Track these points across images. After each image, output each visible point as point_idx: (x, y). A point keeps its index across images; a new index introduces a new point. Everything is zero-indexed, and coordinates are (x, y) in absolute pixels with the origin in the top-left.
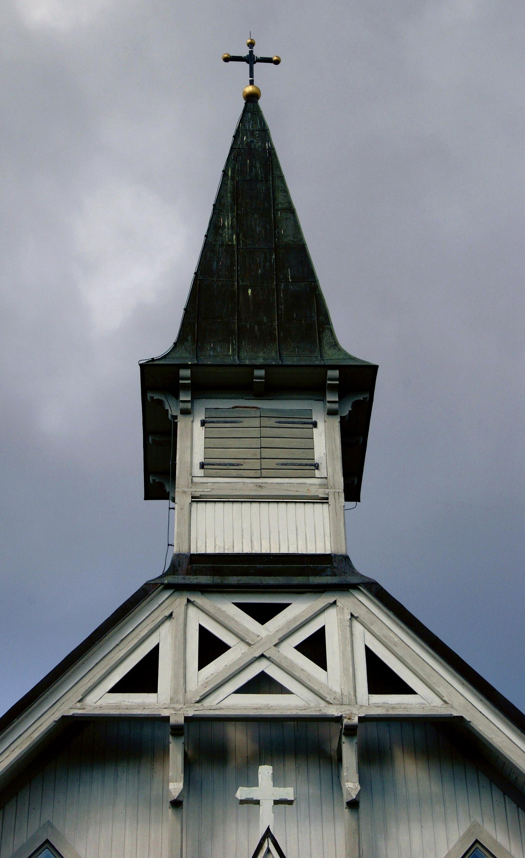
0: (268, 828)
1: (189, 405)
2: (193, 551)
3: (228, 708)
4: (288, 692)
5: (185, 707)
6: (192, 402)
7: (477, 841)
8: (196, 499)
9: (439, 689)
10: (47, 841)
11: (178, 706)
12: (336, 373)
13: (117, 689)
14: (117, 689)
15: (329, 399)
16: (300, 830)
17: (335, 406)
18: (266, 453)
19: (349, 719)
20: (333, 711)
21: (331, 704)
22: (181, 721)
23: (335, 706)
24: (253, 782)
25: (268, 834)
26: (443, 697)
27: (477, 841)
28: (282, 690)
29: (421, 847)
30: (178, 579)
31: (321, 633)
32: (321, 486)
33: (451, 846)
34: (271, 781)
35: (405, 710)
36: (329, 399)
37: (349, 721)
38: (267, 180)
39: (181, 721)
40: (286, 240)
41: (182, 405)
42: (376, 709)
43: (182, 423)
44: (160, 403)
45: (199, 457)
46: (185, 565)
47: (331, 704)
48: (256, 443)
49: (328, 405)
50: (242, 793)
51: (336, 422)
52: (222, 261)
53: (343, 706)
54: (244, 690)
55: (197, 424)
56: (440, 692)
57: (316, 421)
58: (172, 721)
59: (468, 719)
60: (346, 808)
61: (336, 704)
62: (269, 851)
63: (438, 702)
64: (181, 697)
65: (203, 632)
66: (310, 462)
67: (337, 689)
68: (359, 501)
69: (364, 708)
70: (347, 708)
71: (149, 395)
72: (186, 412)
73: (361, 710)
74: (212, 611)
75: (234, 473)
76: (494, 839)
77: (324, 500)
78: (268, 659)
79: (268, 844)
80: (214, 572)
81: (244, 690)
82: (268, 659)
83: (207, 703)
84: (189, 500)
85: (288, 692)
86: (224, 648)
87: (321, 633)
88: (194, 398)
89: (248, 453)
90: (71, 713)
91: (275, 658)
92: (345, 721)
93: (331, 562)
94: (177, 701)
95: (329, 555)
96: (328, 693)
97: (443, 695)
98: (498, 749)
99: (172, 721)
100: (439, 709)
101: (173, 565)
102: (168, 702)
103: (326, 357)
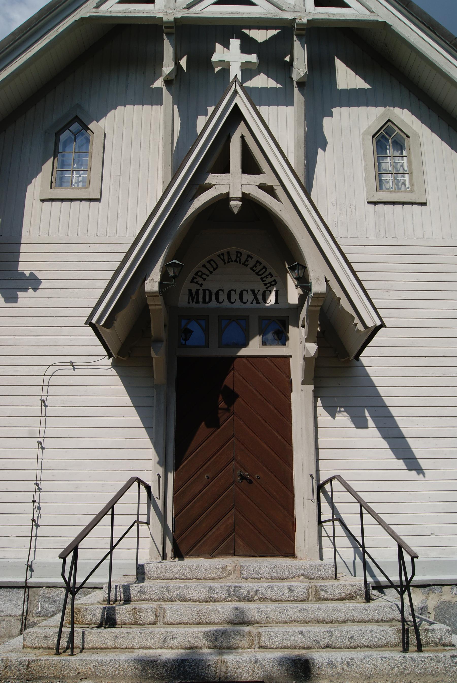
0: (236, 76)
3: (208, 13)
5: (175, 11)
7: (389, 120)
10: (77, 117)
19: (300, 20)
21: (287, 11)
23: (290, 13)
26: (372, 8)
27: (389, 120)
29: (349, 124)
34: (240, 168)
35: (343, 16)
37: (300, 21)
42: (320, 15)
47: (287, 11)
52: (239, 599)
53: (295, 13)
56: (370, 5)
59: (390, 24)
60: (296, 87)
61: (290, 12)
62: (236, 92)
64: (172, 5)
68: (228, 193)
69: (311, 14)
70: (299, 14)
73: (309, 16)
76: (401, 119)
83: (192, 10)
94: (169, 7)
96: (284, 4)
97: (372, 7)
98: (413, 44)
100: (368, 16)
102: (163, 8)
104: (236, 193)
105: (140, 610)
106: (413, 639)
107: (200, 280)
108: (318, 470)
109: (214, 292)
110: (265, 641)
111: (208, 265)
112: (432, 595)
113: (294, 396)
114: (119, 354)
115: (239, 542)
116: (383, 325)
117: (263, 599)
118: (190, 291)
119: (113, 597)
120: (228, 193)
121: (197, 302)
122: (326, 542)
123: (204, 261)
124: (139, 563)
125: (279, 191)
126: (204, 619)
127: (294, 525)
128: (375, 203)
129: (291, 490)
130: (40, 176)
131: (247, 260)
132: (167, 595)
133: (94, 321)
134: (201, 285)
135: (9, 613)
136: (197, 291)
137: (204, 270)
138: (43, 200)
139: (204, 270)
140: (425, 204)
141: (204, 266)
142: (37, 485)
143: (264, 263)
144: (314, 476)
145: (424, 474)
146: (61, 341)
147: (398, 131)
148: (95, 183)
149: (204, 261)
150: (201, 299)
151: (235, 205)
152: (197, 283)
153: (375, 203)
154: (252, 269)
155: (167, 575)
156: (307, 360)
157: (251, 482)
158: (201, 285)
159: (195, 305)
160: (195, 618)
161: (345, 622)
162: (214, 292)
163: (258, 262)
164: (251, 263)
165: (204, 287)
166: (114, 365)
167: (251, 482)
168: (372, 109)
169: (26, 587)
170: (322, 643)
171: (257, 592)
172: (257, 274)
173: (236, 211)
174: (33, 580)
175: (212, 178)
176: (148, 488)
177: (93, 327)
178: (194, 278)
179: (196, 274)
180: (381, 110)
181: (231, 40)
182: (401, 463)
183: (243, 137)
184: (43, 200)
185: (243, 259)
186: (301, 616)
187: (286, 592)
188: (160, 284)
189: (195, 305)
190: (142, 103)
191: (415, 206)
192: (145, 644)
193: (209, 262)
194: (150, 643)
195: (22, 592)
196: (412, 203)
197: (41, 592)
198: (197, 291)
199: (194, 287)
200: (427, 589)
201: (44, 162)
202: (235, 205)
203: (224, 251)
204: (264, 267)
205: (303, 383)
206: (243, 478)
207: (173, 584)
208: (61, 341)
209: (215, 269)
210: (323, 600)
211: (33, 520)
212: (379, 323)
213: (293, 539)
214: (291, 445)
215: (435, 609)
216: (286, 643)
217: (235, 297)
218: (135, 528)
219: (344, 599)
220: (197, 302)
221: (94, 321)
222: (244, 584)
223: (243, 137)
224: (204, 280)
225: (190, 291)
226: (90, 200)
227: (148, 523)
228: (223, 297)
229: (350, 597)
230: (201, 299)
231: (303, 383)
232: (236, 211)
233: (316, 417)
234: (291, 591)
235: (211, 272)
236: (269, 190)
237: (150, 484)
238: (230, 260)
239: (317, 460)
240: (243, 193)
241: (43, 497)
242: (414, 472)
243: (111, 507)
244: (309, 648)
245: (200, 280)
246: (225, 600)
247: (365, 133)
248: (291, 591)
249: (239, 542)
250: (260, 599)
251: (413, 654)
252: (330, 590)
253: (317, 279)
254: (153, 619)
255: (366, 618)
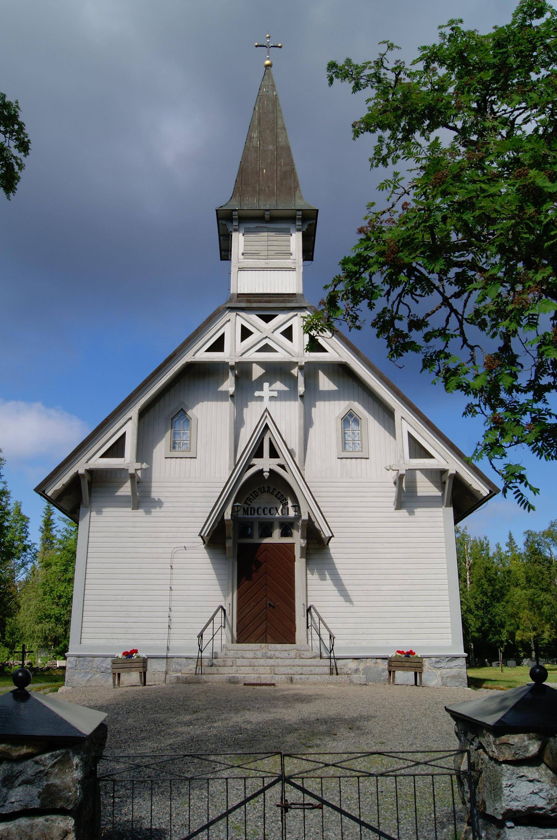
1: (237, 227)
2: (239, 292)
3: (252, 358)
4: (275, 351)
6: (239, 225)
8: (241, 269)
9: (337, 351)
11: (233, 358)
12: (300, 213)
13: (208, 350)
14: (208, 350)
15: (297, 224)
16: (229, 618)
17: (300, 227)
18: (270, 248)
20: (295, 360)
22: (234, 364)
24: (261, 389)
25: (266, 410)
28: (275, 351)
30: (232, 305)
31: (290, 328)
32: (293, 263)
33: (341, 411)
36: (297, 224)
38: (274, 112)
39: (234, 364)
40: (281, 144)
41: (234, 227)
43: (234, 235)
44: (225, 225)
45: (241, 250)
46: (235, 298)
48: (266, 243)
49: (297, 227)
50: (257, 394)
51: (300, 234)
54: (260, 350)
55: (241, 234)
57: (327, 66)
58: (230, 364)
62: (266, 416)
63: (337, 356)
64: (233, 354)
65: (243, 327)
66: (289, 252)
67: (297, 350)
68: (263, 469)
71: (220, 222)
72: (236, 230)
74: (246, 318)
75: (256, 257)
77: (294, 270)
78: (269, 338)
79: (266, 414)
80: (249, 301)
81: (260, 350)
82: (269, 338)
83: (244, 356)
84: (237, 269)
85: (275, 351)
86: (251, 333)
87: (290, 328)
88: (239, 223)
89: (262, 248)
90: (190, 361)
91: (271, 338)
92: (299, 364)
93: (296, 297)
95: (295, 294)
99: (230, 364)
101: (230, 299)
103: (297, 204)
104: (266, 469)
105: (226, 661)
106: (334, 671)
107: (249, 503)
108: (307, 601)
109: (256, 509)
110: (276, 672)
111: (253, 494)
112: (362, 663)
113: (296, 563)
114: (209, 542)
115: (269, 637)
116: (333, 536)
117: (277, 658)
118: (244, 508)
119: (197, 672)
120: (263, 469)
121: (248, 514)
122: (310, 636)
123: (251, 492)
124: (214, 651)
125: (287, 468)
126: (252, 664)
127: (295, 628)
128: (341, 458)
129: (294, 611)
130: (164, 440)
131: (273, 491)
132: (236, 656)
133: (202, 535)
134: (249, 505)
135: (159, 670)
136: (248, 508)
137: (251, 497)
138: (166, 458)
139: (251, 497)
140: (368, 458)
141: (251, 494)
142: (170, 608)
143: (282, 493)
144: (305, 604)
145: (353, 604)
146: (179, 535)
147: (355, 415)
148: (193, 448)
149: (251, 492)
150: (249, 513)
151: (266, 475)
152: (247, 504)
153: (341, 458)
154: (276, 496)
155: (236, 649)
156: (302, 548)
157: (274, 607)
158: (249, 505)
159: (246, 516)
160: (249, 664)
161: (310, 666)
162: (256, 509)
163: (279, 492)
164: (275, 493)
165: (252, 506)
166: (206, 548)
167: (274, 607)
168: (342, 402)
169: (167, 658)
170: (299, 673)
171: (274, 655)
172: (278, 499)
173: (266, 478)
174: (170, 654)
175: (255, 461)
176: (224, 611)
177: (202, 537)
178: (246, 501)
179: (247, 499)
180: (346, 403)
181: (264, 371)
182: (342, 599)
183: (270, 438)
184: (166, 458)
185: (271, 490)
186: (292, 663)
187: (287, 655)
188: (232, 515)
189: (246, 516)
190: (217, 400)
191: (363, 459)
192: (229, 672)
193: (253, 492)
194: (231, 672)
195: (165, 660)
196: (361, 458)
197: (174, 660)
198: (248, 508)
199: (246, 506)
200: (359, 660)
201: (166, 431)
202: (266, 475)
203: (261, 486)
204: (282, 495)
205: (301, 558)
206: (270, 605)
207: (239, 652)
208: (179, 535)
209: (256, 496)
210: (302, 658)
211: (169, 626)
212: (331, 535)
213: (294, 635)
214: (294, 589)
215: (363, 670)
216: (285, 672)
217: (267, 511)
218: (220, 630)
219: (311, 658)
220: (248, 514)
221: (202, 535)
222: (269, 652)
223: (270, 438)
224: (251, 502)
225: (244, 508)
226: (191, 458)
227: (224, 627)
228: (261, 511)
229: (314, 657)
230: (249, 513)
231: (301, 558)
232: (266, 478)
233: (306, 575)
234: (289, 654)
235: (255, 498)
236: (282, 467)
237: (225, 608)
238: (264, 491)
239: (307, 596)
240: (270, 469)
241: (172, 614)
242: (348, 603)
243: (212, 618)
244: (294, 674)
245: (249, 503)
246: (261, 658)
247: (337, 417)
248: (289, 654)
249: (269, 637)
250: (276, 658)
251: (334, 676)
252: (305, 654)
253: (304, 512)
254: (231, 664)
255: (319, 665)
